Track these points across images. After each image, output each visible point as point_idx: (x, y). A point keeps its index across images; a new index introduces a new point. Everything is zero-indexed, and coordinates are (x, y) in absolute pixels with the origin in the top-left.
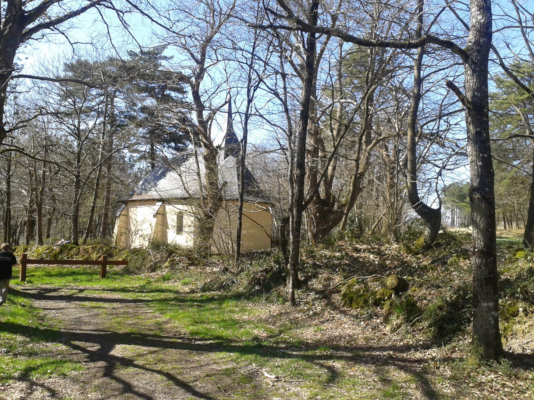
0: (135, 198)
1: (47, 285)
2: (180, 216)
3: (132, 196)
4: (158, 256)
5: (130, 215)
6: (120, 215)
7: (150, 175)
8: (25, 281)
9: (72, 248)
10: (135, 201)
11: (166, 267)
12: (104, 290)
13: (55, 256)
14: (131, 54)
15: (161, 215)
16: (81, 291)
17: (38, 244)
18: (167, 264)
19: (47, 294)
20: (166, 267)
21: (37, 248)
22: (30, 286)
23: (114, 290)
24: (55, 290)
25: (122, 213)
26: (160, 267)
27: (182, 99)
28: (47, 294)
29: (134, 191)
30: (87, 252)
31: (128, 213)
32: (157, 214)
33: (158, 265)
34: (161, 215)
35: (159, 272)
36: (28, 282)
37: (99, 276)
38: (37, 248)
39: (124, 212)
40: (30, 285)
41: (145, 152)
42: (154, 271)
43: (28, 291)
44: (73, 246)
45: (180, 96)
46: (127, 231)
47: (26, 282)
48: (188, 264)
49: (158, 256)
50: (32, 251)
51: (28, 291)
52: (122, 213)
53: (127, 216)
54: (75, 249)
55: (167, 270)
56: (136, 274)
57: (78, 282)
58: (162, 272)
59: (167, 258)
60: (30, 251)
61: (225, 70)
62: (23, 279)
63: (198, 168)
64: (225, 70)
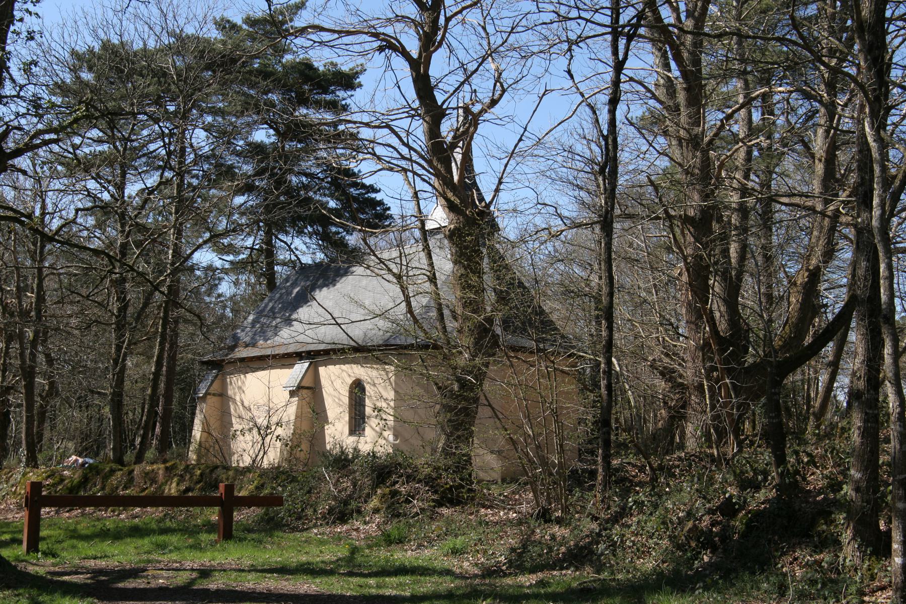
0: (242, 353)
1: (98, 562)
2: (358, 389)
3: (232, 348)
4: (347, 484)
5: (230, 392)
6: (206, 394)
7: (270, 301)
8: (37, 551)
9: (112, 472)
10: (242, 360)
11: (376, 511)
12: (253, 569)
13: (73, 489)
14: (225, 25)
15: (309, 392)
16: (205, 573)
17: (27, 465)
18: (374, 502)
19: (121, 585)
20: (376, 511)
21: (24, 474)
22: (53, 565)
23: (283, 570)
24: (134, 573)
25: (212, 390)
26: (359, 512)
27: (335, 125)
28: (121, 585)
29: (236, 338)
30: (153, 481)
31: (224, 386)
32: (300, 387)
33: (353, 505)
34: (309, 392)
35: (357, 524)
36: (45, 554)
37: (213, 537)
38: (24, 474)
39: (216, 387)
40: (52, 560)
41: (252, 249)
42: (343, 517)
43: (66, 578)
44: (114, 466)
45: (329, 117)
46: (222, 434)
47: (40, 555)
48: (433, 500)
49: (347, 484)
50: (12, 482)
51: (66, 578)
52: (212, 390)
53: (223, 396)
54: (119, 473)
55: (378, 518)
56: (294, 529)
57: (171, 551)
58: (366, 523)
59: (374, 488)
60: (7, 482)
61: (484, 28)
62: (33, 546)
63: (431, 264)
64: (484, 28)
